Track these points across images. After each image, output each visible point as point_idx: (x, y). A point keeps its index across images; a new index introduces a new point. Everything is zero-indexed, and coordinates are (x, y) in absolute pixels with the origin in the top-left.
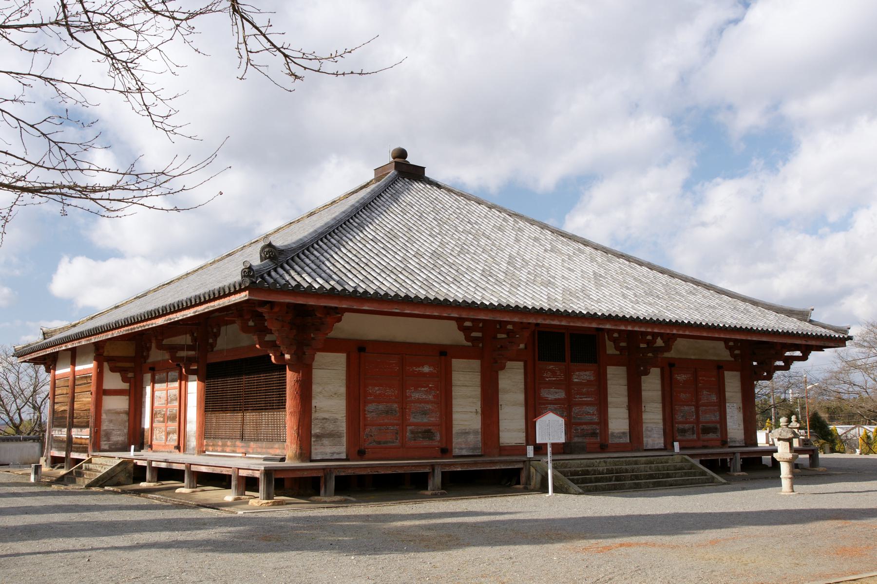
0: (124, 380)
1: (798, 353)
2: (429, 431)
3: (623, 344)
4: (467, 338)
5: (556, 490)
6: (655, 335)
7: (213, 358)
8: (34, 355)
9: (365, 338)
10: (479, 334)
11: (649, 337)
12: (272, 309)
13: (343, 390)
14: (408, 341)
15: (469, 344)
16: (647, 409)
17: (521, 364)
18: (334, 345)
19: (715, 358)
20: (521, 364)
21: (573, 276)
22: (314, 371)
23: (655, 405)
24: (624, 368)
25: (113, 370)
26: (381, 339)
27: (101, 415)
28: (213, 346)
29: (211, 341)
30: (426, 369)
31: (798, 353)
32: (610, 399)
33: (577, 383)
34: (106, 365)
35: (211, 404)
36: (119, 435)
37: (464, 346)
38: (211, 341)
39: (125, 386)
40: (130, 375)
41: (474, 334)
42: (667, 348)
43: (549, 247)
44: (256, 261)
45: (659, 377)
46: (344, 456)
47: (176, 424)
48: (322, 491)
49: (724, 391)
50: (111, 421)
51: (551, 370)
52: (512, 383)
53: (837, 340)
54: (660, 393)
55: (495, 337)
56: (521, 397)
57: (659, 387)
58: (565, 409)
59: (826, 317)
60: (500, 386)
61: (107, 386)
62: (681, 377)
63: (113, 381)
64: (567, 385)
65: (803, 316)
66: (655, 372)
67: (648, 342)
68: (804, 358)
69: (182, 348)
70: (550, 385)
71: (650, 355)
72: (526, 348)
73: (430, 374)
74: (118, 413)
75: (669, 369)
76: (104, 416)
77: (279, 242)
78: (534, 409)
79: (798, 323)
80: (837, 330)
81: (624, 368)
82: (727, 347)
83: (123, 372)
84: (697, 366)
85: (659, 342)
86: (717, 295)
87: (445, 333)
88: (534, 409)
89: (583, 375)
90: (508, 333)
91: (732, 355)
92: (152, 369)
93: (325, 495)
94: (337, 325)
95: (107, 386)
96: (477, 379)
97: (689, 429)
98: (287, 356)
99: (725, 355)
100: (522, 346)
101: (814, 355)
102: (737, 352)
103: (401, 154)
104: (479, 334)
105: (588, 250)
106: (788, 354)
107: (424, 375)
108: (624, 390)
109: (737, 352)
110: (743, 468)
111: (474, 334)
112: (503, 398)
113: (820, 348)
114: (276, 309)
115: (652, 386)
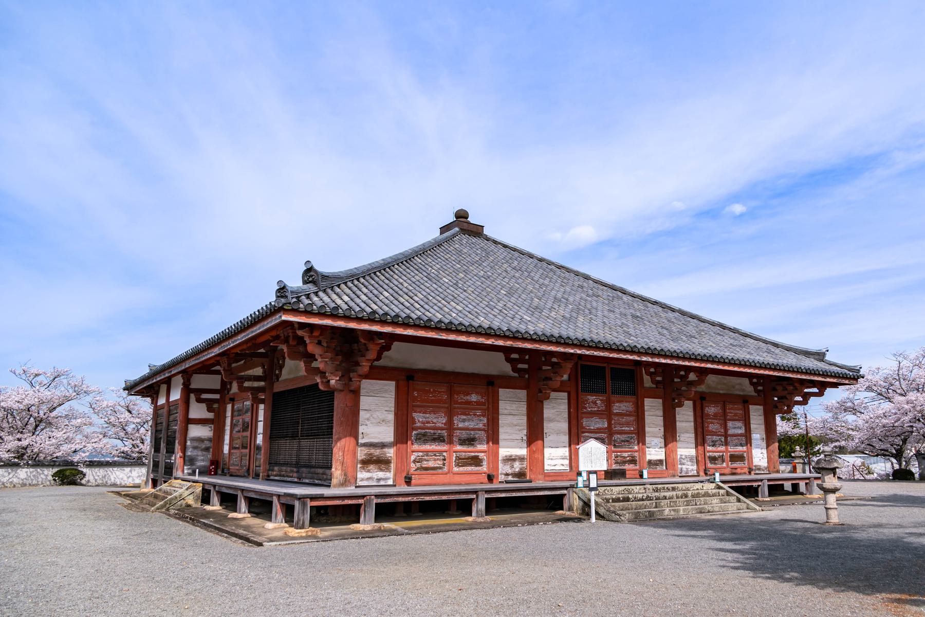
0: (210, 409)
1: (815, 390)
2: (476, 458)
3: (659, 379)
4: (514, 369)
5: (599, 516)
6: (689, 369)
7: (278, 388)
8: (734, 485)
9: (415, 367)
10: (526, 366)
11: (682, 373)
12: (312, 332)
13: (391, 417)
14: (457, 370)
15: (516, 375)
16: (682, 439)
17: (566, 394)
18: (378, 373)
19: (741, 393)
20: (566, 394)
21: (612, 315)
22: (362, 398)
23: (688, 435)
24: (661, 400)
25: (199, 400)
26: (429, 368)
27: (185, 442)
28: (278, 377)
29: (277, 372)
30: (474, 398)
31: (815, 390)
32: (647, 429)
33: (617, 414)
34: (192, 396)
35: (275, 432)
36: (203, 460)
37: (510, 377)
38: (277, 372)
39: (211, 415)
40: (216, 406)
41: (520, 366)
42: (700, 382)
43: (590, 292)
44: (295, 282)
45: (692, 409)
46: (390, 482)
47: (247, 451)
48: (362, 519)
49: (749, 424)
50: (195, 448)
51: (595, 402)
52: (556, 413)
53: (851, 377)
54: (692, 424)
55: (540, 369)
56: (565, 426)
57: (692, 418)
58: (607, 437)
59: (839, 357)
60: (545, 416)
61: (193, 415)
62: (711, 410)
63: (197, 411)
64: (608, 413)
65: (820, 356)
66: (688, 404)
67: (681, 377)
68: (820, 394)
69: (249, 378)
70: (592, 414)
71: (684, 388)
72: (569, 379)
73: (478, 403)
74: (200, 440)
75: (700, 402)
76: (189, 443)
77: (322, 267)
78: (576, 436)
79: (816, 362)
80: (850, 369)
81: (661, 400)
82: (752, 383)
83: (210, 404)
84: (724, 400)
85: (692, 377)
86: (742, 337)
87: (498, 365)
88: (576, 436)
89: (622, 406)
90: (553, 365)
91: (756, 391)
92: (232, 400)
93: (364, 523)
94: (386, 353)
95: (193, 415)
96: (523, 408)
97: (719, 457)
98: (333, 382)
99: (749, 390)
100: (565, 377)
101: (829, 391)
102: (760, 388)
103: (461, 216)
104: (526, 366)
105: (625, 298)
106: (806, 390)
107: (469, 403)
108: (660, 421)
109: (760, 388)
110: (770, 495)
111: (520, 366)
112: (548, 427)
113: (835, 385)
114: (316, 333)
115: (685, 417)
